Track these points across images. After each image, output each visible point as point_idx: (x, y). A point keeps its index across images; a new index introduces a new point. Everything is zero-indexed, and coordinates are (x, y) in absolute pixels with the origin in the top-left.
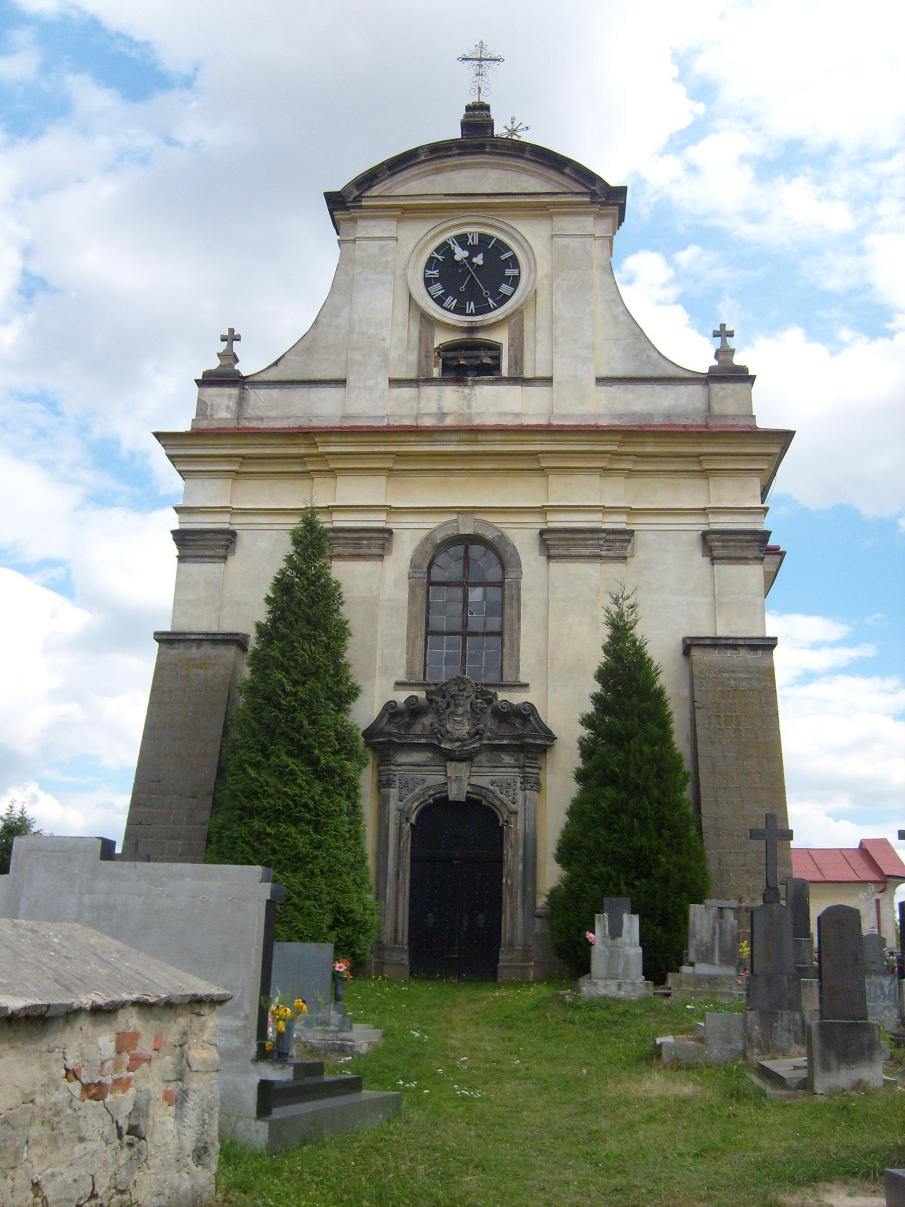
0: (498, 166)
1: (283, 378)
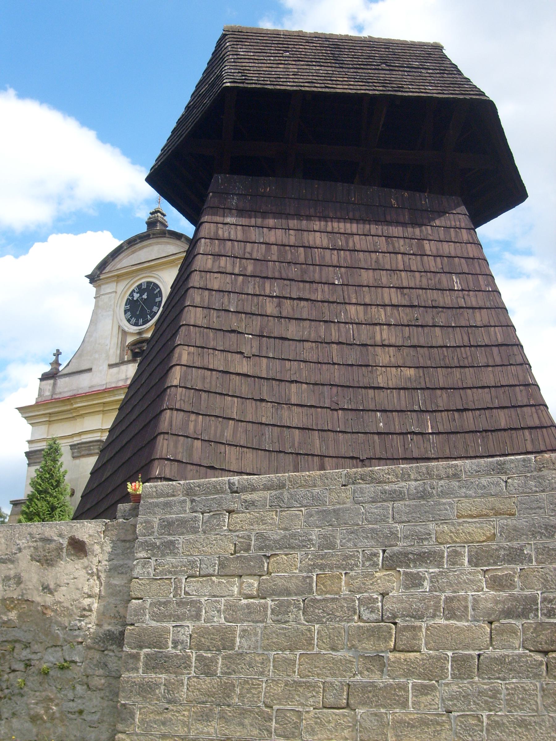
0: (158, 243)
1: (70, 371)
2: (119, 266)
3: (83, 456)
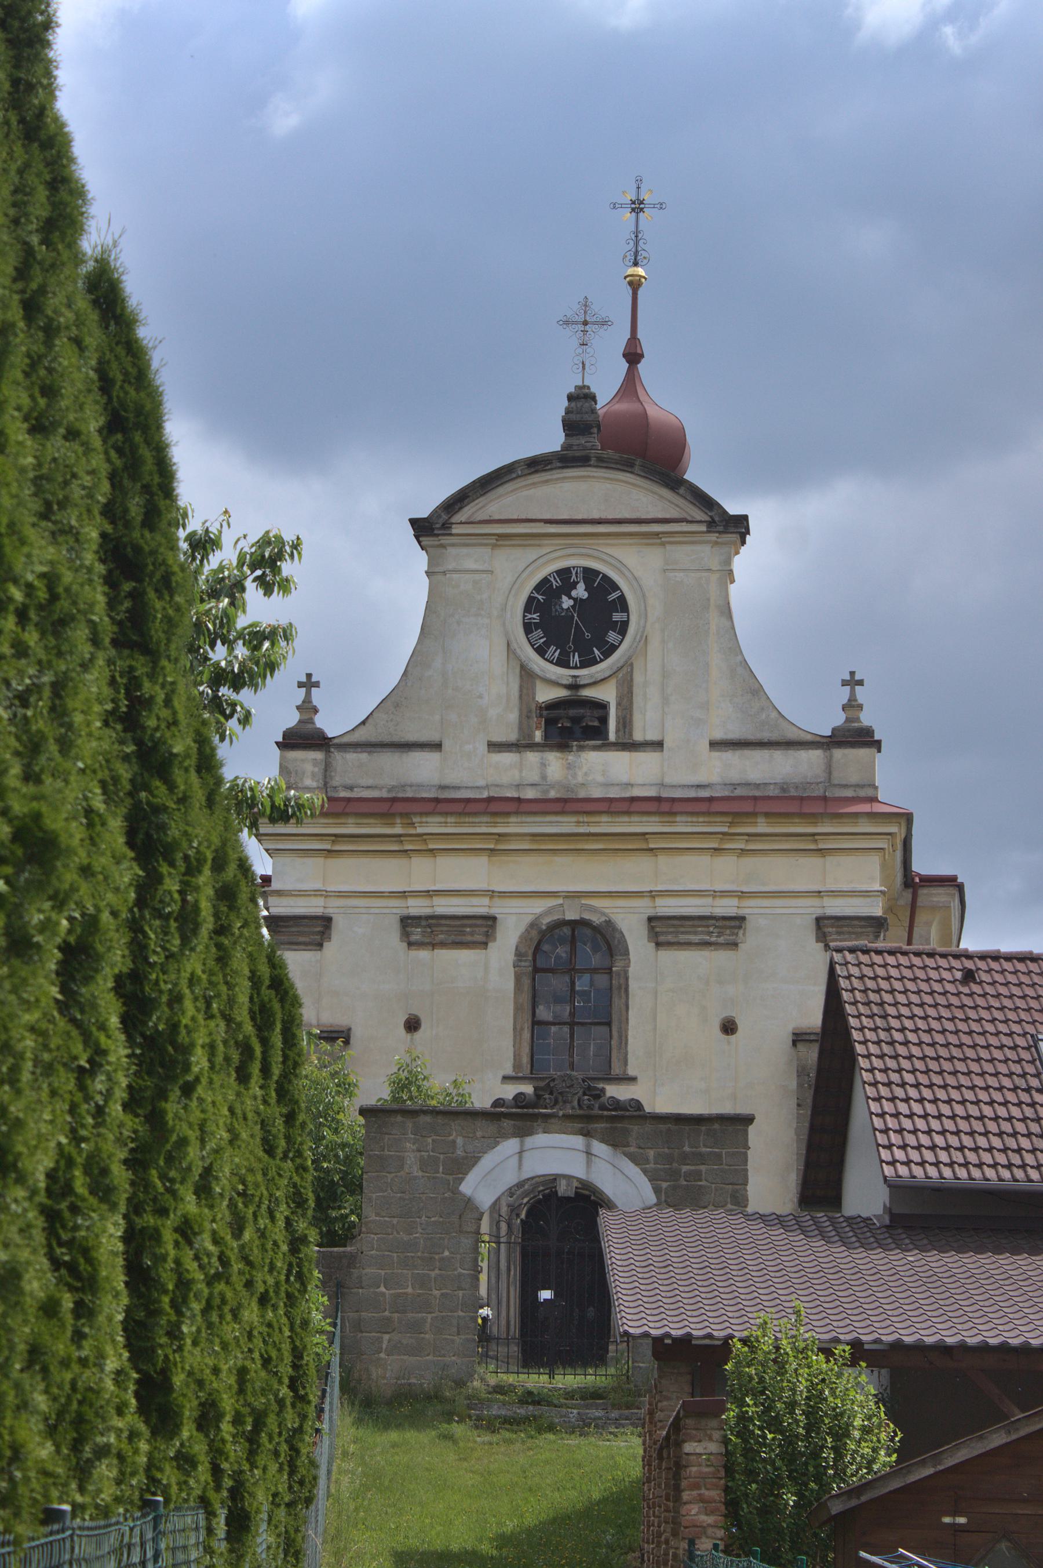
2: (608, 550)
3: (443, 945)
